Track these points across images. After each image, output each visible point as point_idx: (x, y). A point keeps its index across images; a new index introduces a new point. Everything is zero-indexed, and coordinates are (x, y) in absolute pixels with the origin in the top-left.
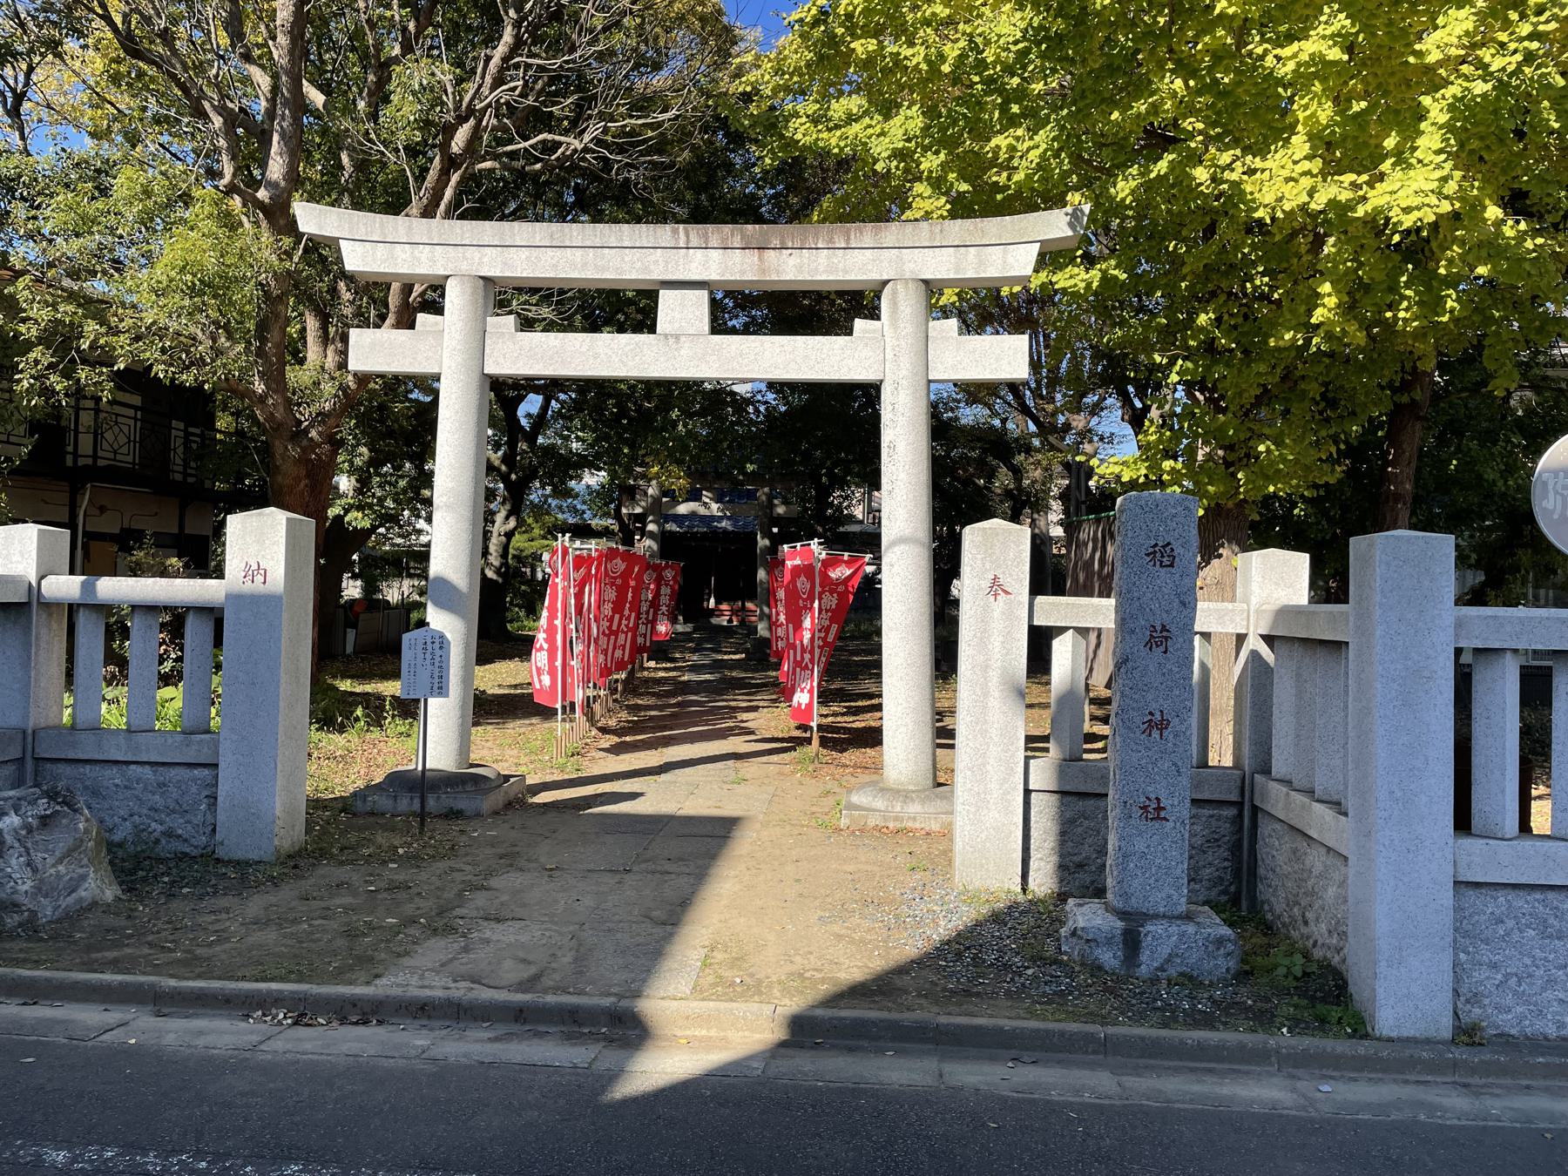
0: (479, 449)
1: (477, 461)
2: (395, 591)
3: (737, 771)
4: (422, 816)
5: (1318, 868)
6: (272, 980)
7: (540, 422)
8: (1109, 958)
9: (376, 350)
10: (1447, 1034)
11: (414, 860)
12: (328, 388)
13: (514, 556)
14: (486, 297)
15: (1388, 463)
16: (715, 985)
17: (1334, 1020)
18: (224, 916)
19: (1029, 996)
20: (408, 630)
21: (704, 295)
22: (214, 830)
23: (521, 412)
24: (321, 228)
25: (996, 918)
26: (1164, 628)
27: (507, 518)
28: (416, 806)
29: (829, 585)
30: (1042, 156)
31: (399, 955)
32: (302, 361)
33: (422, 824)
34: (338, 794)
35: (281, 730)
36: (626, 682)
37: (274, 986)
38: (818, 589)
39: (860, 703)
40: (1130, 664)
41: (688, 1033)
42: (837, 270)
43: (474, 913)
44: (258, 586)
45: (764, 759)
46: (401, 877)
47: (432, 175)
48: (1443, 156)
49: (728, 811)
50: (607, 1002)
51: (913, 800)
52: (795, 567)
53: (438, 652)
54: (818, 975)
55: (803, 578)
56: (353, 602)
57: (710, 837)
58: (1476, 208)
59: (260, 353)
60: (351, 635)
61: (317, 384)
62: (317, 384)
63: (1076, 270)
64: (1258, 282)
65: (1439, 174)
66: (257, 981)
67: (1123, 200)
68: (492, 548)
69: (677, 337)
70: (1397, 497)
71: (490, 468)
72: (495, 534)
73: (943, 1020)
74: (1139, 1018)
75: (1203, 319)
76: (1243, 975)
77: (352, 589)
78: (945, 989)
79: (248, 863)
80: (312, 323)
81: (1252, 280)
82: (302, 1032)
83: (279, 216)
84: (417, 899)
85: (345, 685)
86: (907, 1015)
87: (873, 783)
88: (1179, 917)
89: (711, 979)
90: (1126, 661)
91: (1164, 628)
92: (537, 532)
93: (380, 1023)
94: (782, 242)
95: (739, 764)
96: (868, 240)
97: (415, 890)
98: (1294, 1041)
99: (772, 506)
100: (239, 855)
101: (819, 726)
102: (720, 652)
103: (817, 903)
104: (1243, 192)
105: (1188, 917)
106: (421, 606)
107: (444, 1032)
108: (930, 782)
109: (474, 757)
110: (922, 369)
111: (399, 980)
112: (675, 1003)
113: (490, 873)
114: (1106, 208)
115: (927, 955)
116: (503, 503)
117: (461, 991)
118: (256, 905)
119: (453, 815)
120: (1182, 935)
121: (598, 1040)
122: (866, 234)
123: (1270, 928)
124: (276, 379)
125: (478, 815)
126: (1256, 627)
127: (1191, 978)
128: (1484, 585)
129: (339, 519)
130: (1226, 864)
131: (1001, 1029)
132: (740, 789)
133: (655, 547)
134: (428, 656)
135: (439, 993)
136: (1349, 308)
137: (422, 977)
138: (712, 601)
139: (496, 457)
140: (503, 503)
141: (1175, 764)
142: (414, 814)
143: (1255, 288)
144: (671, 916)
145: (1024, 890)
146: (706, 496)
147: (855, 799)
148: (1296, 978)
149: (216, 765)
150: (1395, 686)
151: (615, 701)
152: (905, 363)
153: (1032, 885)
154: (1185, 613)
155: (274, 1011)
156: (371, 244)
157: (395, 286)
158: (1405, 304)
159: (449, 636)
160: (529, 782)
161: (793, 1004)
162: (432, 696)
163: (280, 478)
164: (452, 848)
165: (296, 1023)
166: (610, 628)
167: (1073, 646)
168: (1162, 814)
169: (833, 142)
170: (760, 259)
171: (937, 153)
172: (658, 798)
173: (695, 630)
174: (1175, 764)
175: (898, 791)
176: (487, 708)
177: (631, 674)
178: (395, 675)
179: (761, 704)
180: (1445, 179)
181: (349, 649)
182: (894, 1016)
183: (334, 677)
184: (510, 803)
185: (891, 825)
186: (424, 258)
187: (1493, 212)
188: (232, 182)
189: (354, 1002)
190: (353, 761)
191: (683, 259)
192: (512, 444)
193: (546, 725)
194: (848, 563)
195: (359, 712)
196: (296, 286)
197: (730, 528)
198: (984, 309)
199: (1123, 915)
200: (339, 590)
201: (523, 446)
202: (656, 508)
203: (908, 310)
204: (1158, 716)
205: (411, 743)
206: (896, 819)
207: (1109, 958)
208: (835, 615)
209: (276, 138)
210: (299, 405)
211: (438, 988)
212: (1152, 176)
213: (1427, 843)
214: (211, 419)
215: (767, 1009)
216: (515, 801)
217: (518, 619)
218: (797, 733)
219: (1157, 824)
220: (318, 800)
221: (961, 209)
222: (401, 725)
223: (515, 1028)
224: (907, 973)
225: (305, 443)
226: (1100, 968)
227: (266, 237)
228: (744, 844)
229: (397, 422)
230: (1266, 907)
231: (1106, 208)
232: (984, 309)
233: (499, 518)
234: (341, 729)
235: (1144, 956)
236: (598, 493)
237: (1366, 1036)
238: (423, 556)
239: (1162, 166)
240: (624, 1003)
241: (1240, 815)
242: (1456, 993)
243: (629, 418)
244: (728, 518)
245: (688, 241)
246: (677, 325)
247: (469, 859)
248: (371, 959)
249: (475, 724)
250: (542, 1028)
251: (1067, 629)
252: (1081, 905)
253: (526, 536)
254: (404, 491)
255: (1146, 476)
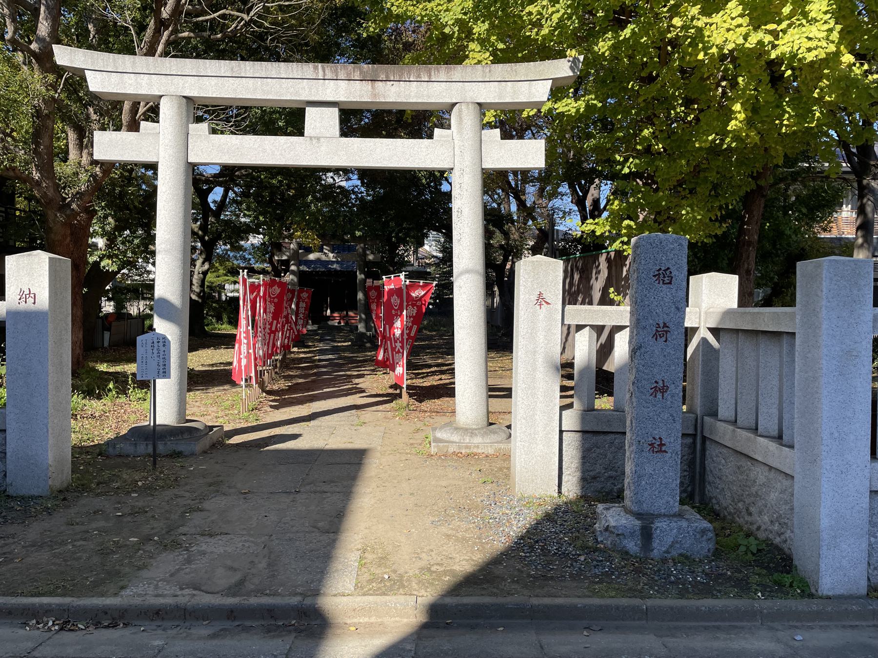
0: (185, 223)
1: (185, 232)
2: (134, 308)
3: (358, 417)
4: (155, 456)
5: (761, 479)
6: (43, 595)
7: (222, 205)
8: (632, 546)
9: (111, 146)
10: (864, 591)
11: (149, 490)
12: (83, 177)
13: (208, 286)
14: (188, 111)
15: (744, 223)
16: (370, 581)
17: (788, 584)
18: (11, 540)
19: (586, 578)
20: (143, 333)
21: (335, 112)
22: (5, 475)
23: (210, 199)
24: (72, 62)
25: (549, 517)
26: (665, 325)
27: (203, 263)
28: (150, 450)
29: (414, 302)
30: (561, 19)
31: (139, 569)
32: (65, 160)
33: (155, 463)
34: (96, 442)
35: (50, 405)
36: (282, 361)
37: (45, 600)
38: (405, 304)
39: (424, 371)
40: (643, 350)
41: (355, 620)
42: (423, 96)
43: (193, 531)
44: (29, 305)
45: (374, 408)
46: (140, 504)
47: (149, 32)
48: (829, 16)
49: (358, 445)
50: (295, 600)
51: (476, 435)
52: (391, 290)
53: (162, 349)
54: (441, 569)
55: (395, 297)
56: (108, 315)
57: (348, 464)
58: (837, 54)
59: (35, 151)
60: (107, 335)
61: (76, 174)
62: (76, 174)
63: (569, 101)
64: (678, 110)
65: (826, 27)
66: (32, 596)
67: (604, 53)
68: (194, 281)
69: (318, 139)
70: (749, 243)
71: (194, 233)
72: (196, 273)
73: (535, 601)
74: (663, 592)
75: (646, 132)
76: (717, 554)
77: (108, 307)
78: (529, 576)
79: (32, 497)
80: (72, 136)
81: (674, 109)
82: (67, 636)
83: (45, 59)
84: (152, 522)
85: (103, 367)
86: (509, 599)
87: (449, 424)
88: (674, 515)
89: (366, 576)
90: (640, 348)
91: (665, 325)
92: (221, 272)
93: (126, 625)
94: (387, 76)
95: (359, 412)
96: (442, 76)
97: (149, 514)
98: (769, 603)
99: (365, 255)
100: (23, 492)
101: (408, 387)
102: (335, 341)
103: (428, 511)
104: (703, 36)
105: (680, 515)
106: (150, 317)
107: (175, 631)
108: (485, 423)
109: (190, 414)
110: (478, 161)
111: (140, 590)
112: (345, 599)
113: (203, 498)
114: (593, 60)
115: (510, 548)
116: (200, 254)
117: (186, 598)
118: (34, 530)
119: (176, 455)
120: (679, 528)
121: (290, 631)
122: (442, 72)
123: (718, 515)
124: (47, 169)
125: (193, 454)
126: (705, 323)
127: (687, 557)
128: (771, 295)
129: (96, 264)
130: (686, 473)
131: (576, 606)
132: (363, 429)
133: (296, 280)
134: (155, 351)
135: (169, 601)
136: (749, 122)
137: (157, 587)
138: (329, 311)
139: (196, 226)
140: (200, 254)
141: (672, 415)
142: (149, 455)
143: (677, 113)
144: (332, 525)
145: (560, 492)
146: (326, 249)
147: (439, 435)
148: (753, 554)
149: (5, 431)
150: (835, 362)
151: (276, 373)
152: (461, 157)
153: (564, 489)
154: (679, 314)
155: (45, 619)
156: (108, 75)
157: (127, 106)
158: (787, 116)
159: (169, 337)
160: (226, 429)
161: (428, 595)
162: (159, 378)
163: (52, 236)
164: (176, 480)
165: (61, 629)
166: (270, 329)
167: (590, 337)
168: (663, 448)
169: (418, 11)
170: (373, 87)
171: (483, 22)
172: (314, 437)
173: (319, 328)
174: (672, 415)
175: (467, 430)
176: (197, 380)
177: (284, 355)
178: (133, 360)
179: (366, 373)
180: (830, 30)
181: (106, 344)
182: (500, 600)
183: (96, 362)
184: (214, 445)
185: (463, 451)
186: (144, 83)
187: (848, 58)
188: (13, 37)
189: (105, 611)
190: (104, 419)
191: (322, 87)
192: (205, 219)
193: (234, 390)
194: (423, 287)
195: (111, 386)
196: (60, 110)
197: (339, 269)
198: (512, 124)
199: (639, 516)
200: (100, 307)
201: (211, 219)
202: (295, 256)
203: (469, 123)
204: (661, 384)
205: (147, 405)
206: (467, 447)
207: (632, 546)
208: (416, 319)
209: (43, 8)
210: (64, 188)
211: (168, 596)
212: (621, 38)
213: (854, 467)
214: (13, 202)
215: (411, 600)
216: (215, 443)
217: (212, 323)
218: (391, 391)
219: (660, 455)
220: (82, 447)
221: (499, 58)
222: (140, 394)
223: (228, 624)
224: (500, 563)
225: (68, 212)
226: (627, 553)
227: (37, 75)
228: (373, 469)
229: (129, 196)
230: (714, 501)
231: (593, 60)
232: (512, 124)
233: (198, 263)
234: (99, 397)
235: (655, 544)
236: (258, 247)
237: (811, 596)
238: (151, 287)
239: (627, 32)
240: (308, 601)
241: (694, 443)
242: (869, 564)
243: (281, 194)
244: (337, 262)
245: (324, 74)
246: (318, 131)
247: (188, 487)
248: (118, 573)
249: (189, 390)
250: (248, 623)
251: (585, 326)
252: (607, 509)
253: (215, 274)
254: (138, 247)
255: (610, 231)
